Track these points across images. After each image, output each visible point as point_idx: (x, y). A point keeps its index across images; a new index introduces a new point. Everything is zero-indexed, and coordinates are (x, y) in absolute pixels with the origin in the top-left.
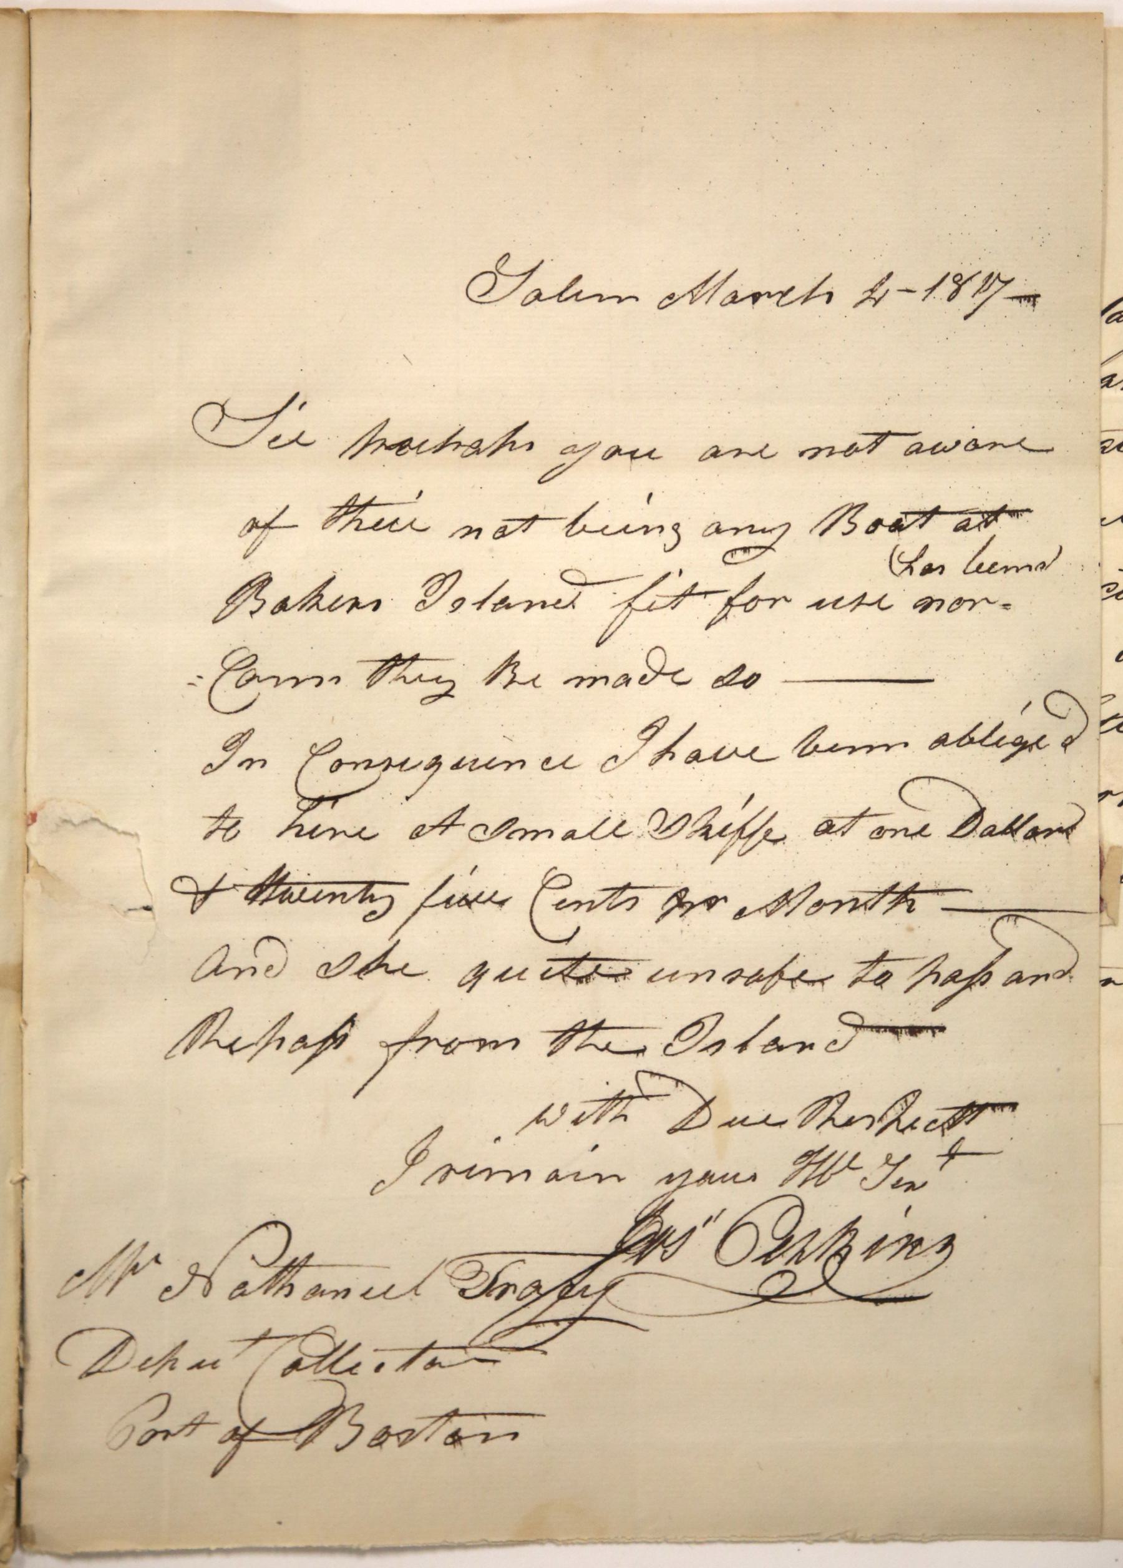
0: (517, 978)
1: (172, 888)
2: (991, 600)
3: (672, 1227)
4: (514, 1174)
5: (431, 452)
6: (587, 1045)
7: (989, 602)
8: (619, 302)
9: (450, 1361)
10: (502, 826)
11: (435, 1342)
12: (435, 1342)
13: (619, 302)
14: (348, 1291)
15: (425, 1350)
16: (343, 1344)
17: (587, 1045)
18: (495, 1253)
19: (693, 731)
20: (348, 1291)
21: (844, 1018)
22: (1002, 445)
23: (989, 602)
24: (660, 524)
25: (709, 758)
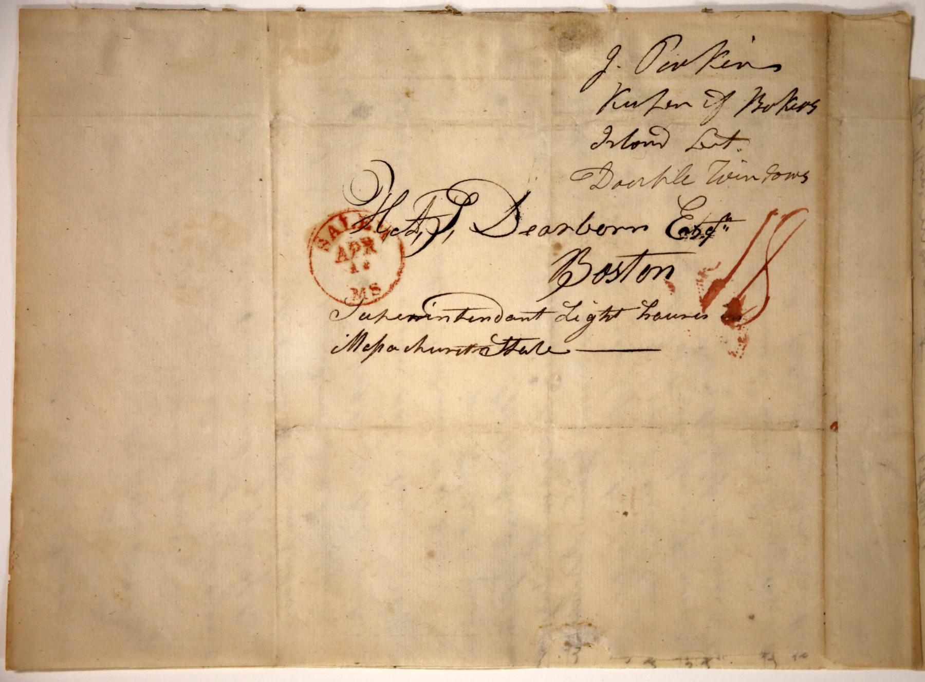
0: (430, 351)
1: (706, 198)
2: (756, 177)
3: (364, 330)
4: (663, 268)
5: (377, 351)
6: (621, 93)
7: (755, 179)
8: (633, 231)
9: (588, 78)
10: (555, 274)
11: (612, 307)
12: (612, 307)
13: (633, 231)
14: (406, 351)
15: (641, 256)
16: (416, 351)
17: (621, 93)
18: (762, 227)
19: (626, 279)
20: (406, 351)
21: (703, 199)
22: (623, 227)
23: (755, 179)
24: (752, 175)
25: (681, 105)
